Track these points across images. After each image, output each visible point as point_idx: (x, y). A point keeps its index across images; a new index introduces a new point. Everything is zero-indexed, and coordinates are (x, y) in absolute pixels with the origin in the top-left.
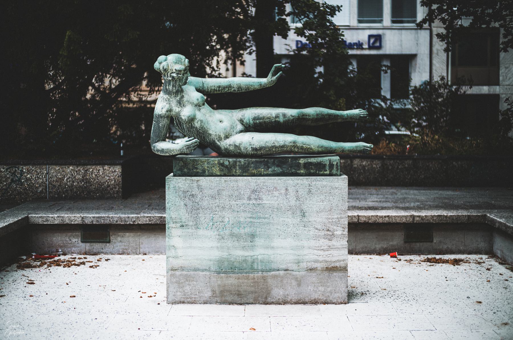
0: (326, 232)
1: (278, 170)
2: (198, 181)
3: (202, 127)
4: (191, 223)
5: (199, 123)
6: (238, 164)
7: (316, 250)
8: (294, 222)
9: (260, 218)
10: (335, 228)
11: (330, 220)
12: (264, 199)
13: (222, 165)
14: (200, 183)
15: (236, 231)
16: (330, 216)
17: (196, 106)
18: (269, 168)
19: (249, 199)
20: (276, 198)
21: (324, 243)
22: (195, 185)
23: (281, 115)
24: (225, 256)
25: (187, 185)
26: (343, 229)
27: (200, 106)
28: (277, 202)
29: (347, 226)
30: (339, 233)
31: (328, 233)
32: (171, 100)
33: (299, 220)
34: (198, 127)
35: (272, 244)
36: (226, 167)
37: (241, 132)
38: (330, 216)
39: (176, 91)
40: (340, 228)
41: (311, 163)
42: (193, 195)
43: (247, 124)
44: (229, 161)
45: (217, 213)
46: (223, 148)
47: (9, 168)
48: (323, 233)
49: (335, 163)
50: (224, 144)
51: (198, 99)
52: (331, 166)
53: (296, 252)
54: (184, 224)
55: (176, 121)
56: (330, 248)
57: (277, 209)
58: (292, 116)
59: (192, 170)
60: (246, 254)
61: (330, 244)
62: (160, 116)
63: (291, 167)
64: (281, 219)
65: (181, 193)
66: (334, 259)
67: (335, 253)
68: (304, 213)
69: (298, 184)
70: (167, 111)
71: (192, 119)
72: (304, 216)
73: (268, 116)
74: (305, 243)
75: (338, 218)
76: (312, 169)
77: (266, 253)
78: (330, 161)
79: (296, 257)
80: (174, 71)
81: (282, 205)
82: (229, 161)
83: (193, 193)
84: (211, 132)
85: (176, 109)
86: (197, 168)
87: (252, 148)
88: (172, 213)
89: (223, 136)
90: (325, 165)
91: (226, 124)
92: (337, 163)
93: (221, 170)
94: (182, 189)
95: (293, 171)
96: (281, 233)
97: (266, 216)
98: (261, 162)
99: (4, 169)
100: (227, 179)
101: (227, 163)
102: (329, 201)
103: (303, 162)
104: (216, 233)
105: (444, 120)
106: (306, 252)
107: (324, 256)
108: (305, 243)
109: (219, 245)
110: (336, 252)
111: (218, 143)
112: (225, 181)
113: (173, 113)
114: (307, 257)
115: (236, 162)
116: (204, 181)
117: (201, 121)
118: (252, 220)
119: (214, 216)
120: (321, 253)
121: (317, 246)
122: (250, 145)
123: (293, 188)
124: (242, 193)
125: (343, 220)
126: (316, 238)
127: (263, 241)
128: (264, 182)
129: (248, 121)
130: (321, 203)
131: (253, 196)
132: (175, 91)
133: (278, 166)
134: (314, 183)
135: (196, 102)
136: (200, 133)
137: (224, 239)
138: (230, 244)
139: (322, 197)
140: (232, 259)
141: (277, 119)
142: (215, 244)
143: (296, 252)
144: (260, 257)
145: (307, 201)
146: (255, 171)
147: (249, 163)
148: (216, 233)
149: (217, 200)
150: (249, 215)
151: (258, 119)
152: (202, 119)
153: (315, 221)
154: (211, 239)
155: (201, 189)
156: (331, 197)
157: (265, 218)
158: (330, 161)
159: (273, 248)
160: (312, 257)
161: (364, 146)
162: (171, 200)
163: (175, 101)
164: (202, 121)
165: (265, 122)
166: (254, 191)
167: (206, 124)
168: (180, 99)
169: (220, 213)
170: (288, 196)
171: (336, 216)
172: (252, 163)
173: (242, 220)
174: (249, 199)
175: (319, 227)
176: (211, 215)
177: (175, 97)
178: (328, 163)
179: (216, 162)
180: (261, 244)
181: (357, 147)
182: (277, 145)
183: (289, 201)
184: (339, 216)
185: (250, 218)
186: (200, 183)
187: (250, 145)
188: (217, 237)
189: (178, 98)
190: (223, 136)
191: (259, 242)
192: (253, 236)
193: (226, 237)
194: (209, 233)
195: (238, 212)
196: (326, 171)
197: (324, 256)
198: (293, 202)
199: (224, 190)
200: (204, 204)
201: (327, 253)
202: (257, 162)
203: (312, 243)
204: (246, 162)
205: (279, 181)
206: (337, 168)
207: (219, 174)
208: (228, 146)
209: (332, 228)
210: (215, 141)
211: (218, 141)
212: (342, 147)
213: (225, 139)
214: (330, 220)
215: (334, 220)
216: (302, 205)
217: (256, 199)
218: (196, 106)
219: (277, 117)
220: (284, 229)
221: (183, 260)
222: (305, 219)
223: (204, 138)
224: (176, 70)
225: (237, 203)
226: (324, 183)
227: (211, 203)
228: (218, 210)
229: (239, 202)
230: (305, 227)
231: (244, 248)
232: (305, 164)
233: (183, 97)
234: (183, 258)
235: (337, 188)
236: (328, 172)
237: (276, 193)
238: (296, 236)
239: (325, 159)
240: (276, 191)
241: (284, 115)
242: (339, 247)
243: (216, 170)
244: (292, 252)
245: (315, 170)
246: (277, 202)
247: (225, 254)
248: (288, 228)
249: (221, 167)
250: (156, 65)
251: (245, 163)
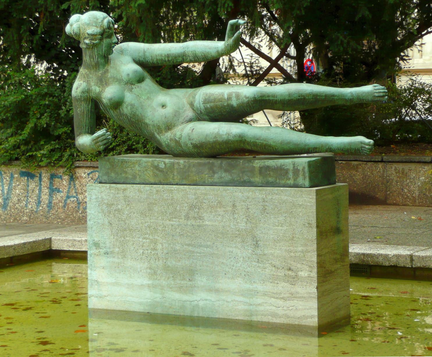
0: (287, 272)
1: (227, 177)
2: (125, 190)
3: (134, 115)
4: (117, 250)
5: (129, 108)
6: (176, 166)
7: (274, 298)
8: (244, 255)
9: (200, 246)
10: (299, 266)
11: (292, 254)
12: (206, 218)
13: (157, 168)
14: (127, 193)
15: (172, 263)
16: (292, 248)
17: (127, 83)
18: (214, 173)
19: (187, 217)
20: (220, 218)
21: (283, 287)
22: (121, 195)
23: (234, 95)
24: (158, 300)
25: (111, 195)
26: (310, 269)
27: (132, 84)
28: (222, 224)
29: (315, 265)
30: (303, 274)
31: (290, 273)
32: (91, 76)
33: (250, 251)
34: (128, 114)
35: (218, 286)
36: (161, 171)
37: (191, 120)
38: (292, 248)
39: (96, 64)
40: (306, 267)
41: (268, 168)
42: (119, 210)
43: (198, 109)
44: (165, 163)
45: (147, 236)
46: (164, 144)
47: (92, 172)
48: (281, 273)
49: (300, 168)
50: (165, 138)
51: (128, 75)
52: (296, 171)
53: (247, 300)
54: (108, 250)
55: (102, 106)
56: (293, 296)
57: (222, 233)
58: (245, 97)
59: (121, 174)
60: (185, 297)
61: (293, 290)
62: (77, 100)
63: (243, 172)
64: (228, 249)
65: (104, 206)
66: (299, 314)
67: (300, 304)
68: (257, 241)
69: (248, 198)
70: (83, 92)
71: (117, 104)
72: (257, 245)
73: (220, 97)
74: (260, 287)
75: (302, 252)
76: (270, 176)
77: (209, 298)
78: (294, 164)
79: (246, 307)
80: (86, 35)
81: (228, 229)
82: (165, 163)
83: (119, 207)
84: (147, 121)
85: (96, 89)
86: (126, 172)
87: (191, 144)
88: (94, 235)
89: (163, 127)
90: (287, 171)
91: (169, 110)
92: (304, 168)
93: (155, 176)
94: (106, 201)
95: (246, 178)
96: (227, 269)
97: (209, 243)
98: (204, 164)
99: (85, 173)
100: (159, 189)
101: (162, 166)
102: (291, 224)
103: (258, 165)
104: (146, 265)
105: (374, 48)
106: (260, 301)
107: (285, 308)
108: (260, 287)
109: (150, 282)
110: (300, 303)
111: (158, 136)
112: (157, 191)
113: (93, 95)
114: (261, 308)
115: (173, 164)
116: (132, 190)
117: (131, 105)
118: (190, 248)
119: (144, 240)
120: (280, 302)
121: (275, 292)
122: (190, 139)
123: (243, 203)
124: (178, 208)
125: (309, 254)
126: (274, 279)
127: (204, 280)
128: (206, 194)
129: (198, 106)
130: (280, 228)
131: (192, 214)
132: (93, 63)
133: (226, 171)
134: (270, 197)
135: (125, 78)
136: (132, 122)
137: (156, 275)
138: (164, 282)
139: (281, 219)
140: (167, 304)
141: (230, 102)
142: (146, 281)
143: (247, 300)
144: (201, 303)
145: (261, 225)
146: (196, 178)
147: (189, 167)
148: (146, 265)
149: (148, 218)
150: (187, 242)
151: (208, 103)
152: (133, 102)
153: (272, 254)
154: (140, 273)
155: (129, 201)
156: (293, 220)
157: (207, 247)
158: (294, 164)
159: (217, 291)
160: (268, 308)
161: (362, 143)
162: (93, 216)
163: (95, 78)
164: (132, 105)
165: (216, 106)
166: (192, 207)
167: (140, 110)
168: (102, 74)
169: (151, 237)
170: (236, 216)
171: (300, 249)
172: (194, 166)
173: (178, 248)
174: (187, 217)
175: (278, 263)
176: (141, 240)
177: (96, 71)
178: (291, 167)
179: (149, 164)
180: (202, 284)
181: (350, 144)
182: (220, 139)
183: (238, 223)
184: (304, 249)
185: (189, 245)
186: (127, 193)
187: (190, 139)
188: (149, 271)
189: (100, 73)
190: (163, 127)
191: (201, 281)
192: (191, 272)
193: (159, 272)
194: (139, 265)
195: (173, 236)
196: (289, 179)
197: (285, 308)
198: (242, 225)
199: (156, 204)
200: (132, 223)
201: (288, 303)
202: (200, 164)
203: (269, 287)
204: (186, 164)
205: (224, 194)
206: (304, 175)
207: (152, 181)
208: (169, 141)
209: (295, 265)
210: (154, 134)
211: (158, 134)
212: (327, 144)
213: (166, 132)
214: (292, 254)
215: (298, 254)
216: (255, 229)
217: (195, 218)
218: (127, 83)
219: (229, 98)
220: (232, 263)
221: (109, 301)
222: (259, 252)
223: (141, 129)
224: (88, 34)
225: (172, 223)
226: (283, 197)
227: (140, 222)
228: (149, 232)
229: (175, 222)
230: (258, 262)
231: (181, 289)
232: (261, 168)
233: (107, 71)
234: (108, 298)
235: (301, 206)
236: (291, 182)
237: (221, 211)
238: (248, 276)
239: (287, 162)
240: (220, 208)
241: (238, 96)
242: (305, 295)
243: (149, 176)
244: (241, 299)
245: (275, 179)
246: (222, 224)
247: (158, 296)
248: (237, 262)
249: (155, 171)
250: (68, 29)
251: (185, 166)
